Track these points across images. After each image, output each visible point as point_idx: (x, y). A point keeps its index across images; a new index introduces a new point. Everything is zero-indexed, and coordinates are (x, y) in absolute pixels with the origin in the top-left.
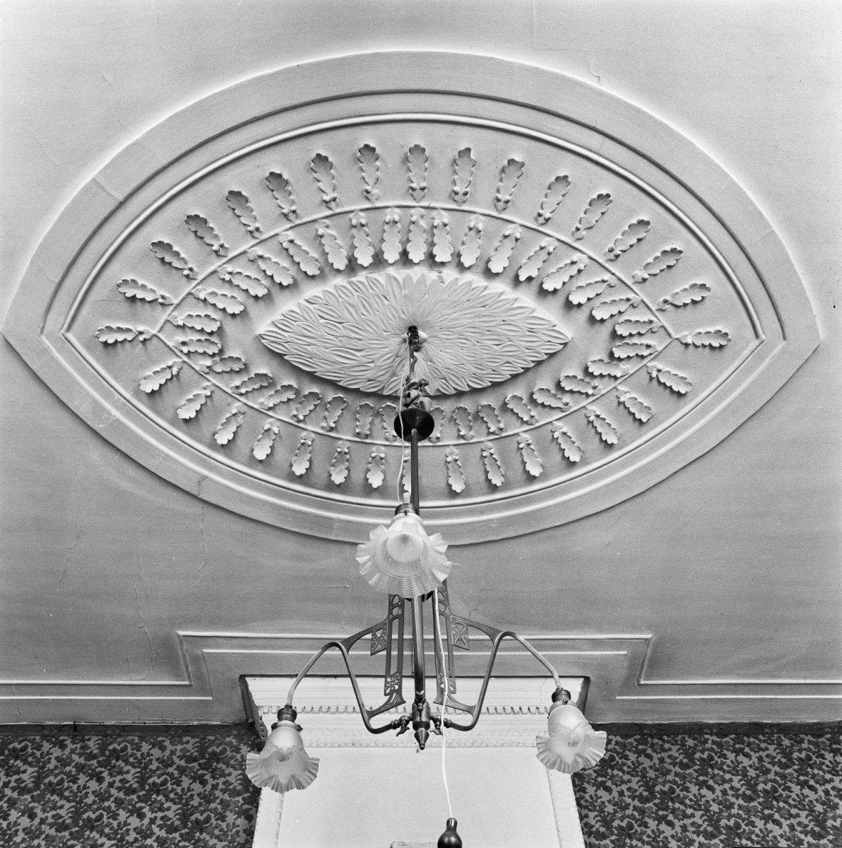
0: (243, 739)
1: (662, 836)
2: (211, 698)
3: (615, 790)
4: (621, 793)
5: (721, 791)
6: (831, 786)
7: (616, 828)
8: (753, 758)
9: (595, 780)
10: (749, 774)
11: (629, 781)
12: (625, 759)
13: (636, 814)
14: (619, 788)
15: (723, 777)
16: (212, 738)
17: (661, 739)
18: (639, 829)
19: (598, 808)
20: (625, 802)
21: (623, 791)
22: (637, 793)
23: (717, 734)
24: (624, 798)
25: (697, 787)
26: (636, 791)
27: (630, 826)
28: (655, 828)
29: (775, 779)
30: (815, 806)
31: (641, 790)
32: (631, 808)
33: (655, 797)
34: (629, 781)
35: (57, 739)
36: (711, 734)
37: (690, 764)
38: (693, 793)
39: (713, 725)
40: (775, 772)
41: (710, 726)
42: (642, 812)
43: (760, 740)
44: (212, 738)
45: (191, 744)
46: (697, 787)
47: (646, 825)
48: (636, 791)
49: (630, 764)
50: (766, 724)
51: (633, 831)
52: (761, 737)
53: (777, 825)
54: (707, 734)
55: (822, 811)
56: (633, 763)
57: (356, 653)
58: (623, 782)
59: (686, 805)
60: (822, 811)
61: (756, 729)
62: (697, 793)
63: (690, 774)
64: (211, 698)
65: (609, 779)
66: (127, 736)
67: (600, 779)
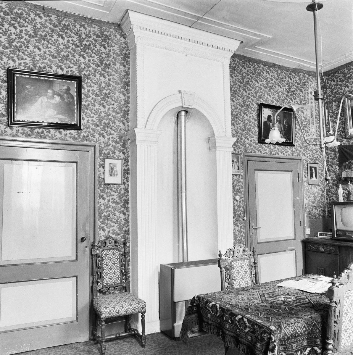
0: (117, 31)
1: (79, 62)
2: (109, 13)
3: (66, 39)
4: (68, 41)
5: (20, 30)
6: (72, 39)
7: (62, 55)
8: (43, 19)
9: (10, 22)
10: (37, 26)
11: (73, 37)
12: (28, 16)
13: (72, 51)
14: (21, 29)
15: (112, 44)
16: (104, 28)
17: (249, 63)
18: (71, 57)
19: (99, 55)
20: (69, 45)
21: (22, 30)
22: (75, 43)
23: (263, 65)
24: (22, 34)
25: (9, 25)
26: (75, 42)
27: (68, 56)
28: (32, 50)
29: (92, 41)
30: (60, 45)
31: (77, 42)
32: (71, 48)
33: (37, 37)
34: (73, 37)
35: (36, 12)
36: (262, 64)
37: (58, 25)
38: (5, 28)
39: (264, 61)
40: (93, 38)
41: (262, 62)
42: (116, 60)
43: (273, 70)
44: (104, 28)
45: (96, 29)
46: (9, 25)
47: (74, 56)
48: (75, 42)
49: (30, 19)
50: (276, 64)
51: (21, 49)
52: (250, 63)
53: (39, 50)
54: (261, 64)
55: (104, 57)
56: (32, 19)
57: (200, 21)
58: (70, 36)
59: (49, 43)
60: (104, 57)
61: (274, 65)
62: (7, 28)
63: (99, 40)
64: (109, 13)
65: (17, 23)
66: (68, 18)
67: (61, 33)
